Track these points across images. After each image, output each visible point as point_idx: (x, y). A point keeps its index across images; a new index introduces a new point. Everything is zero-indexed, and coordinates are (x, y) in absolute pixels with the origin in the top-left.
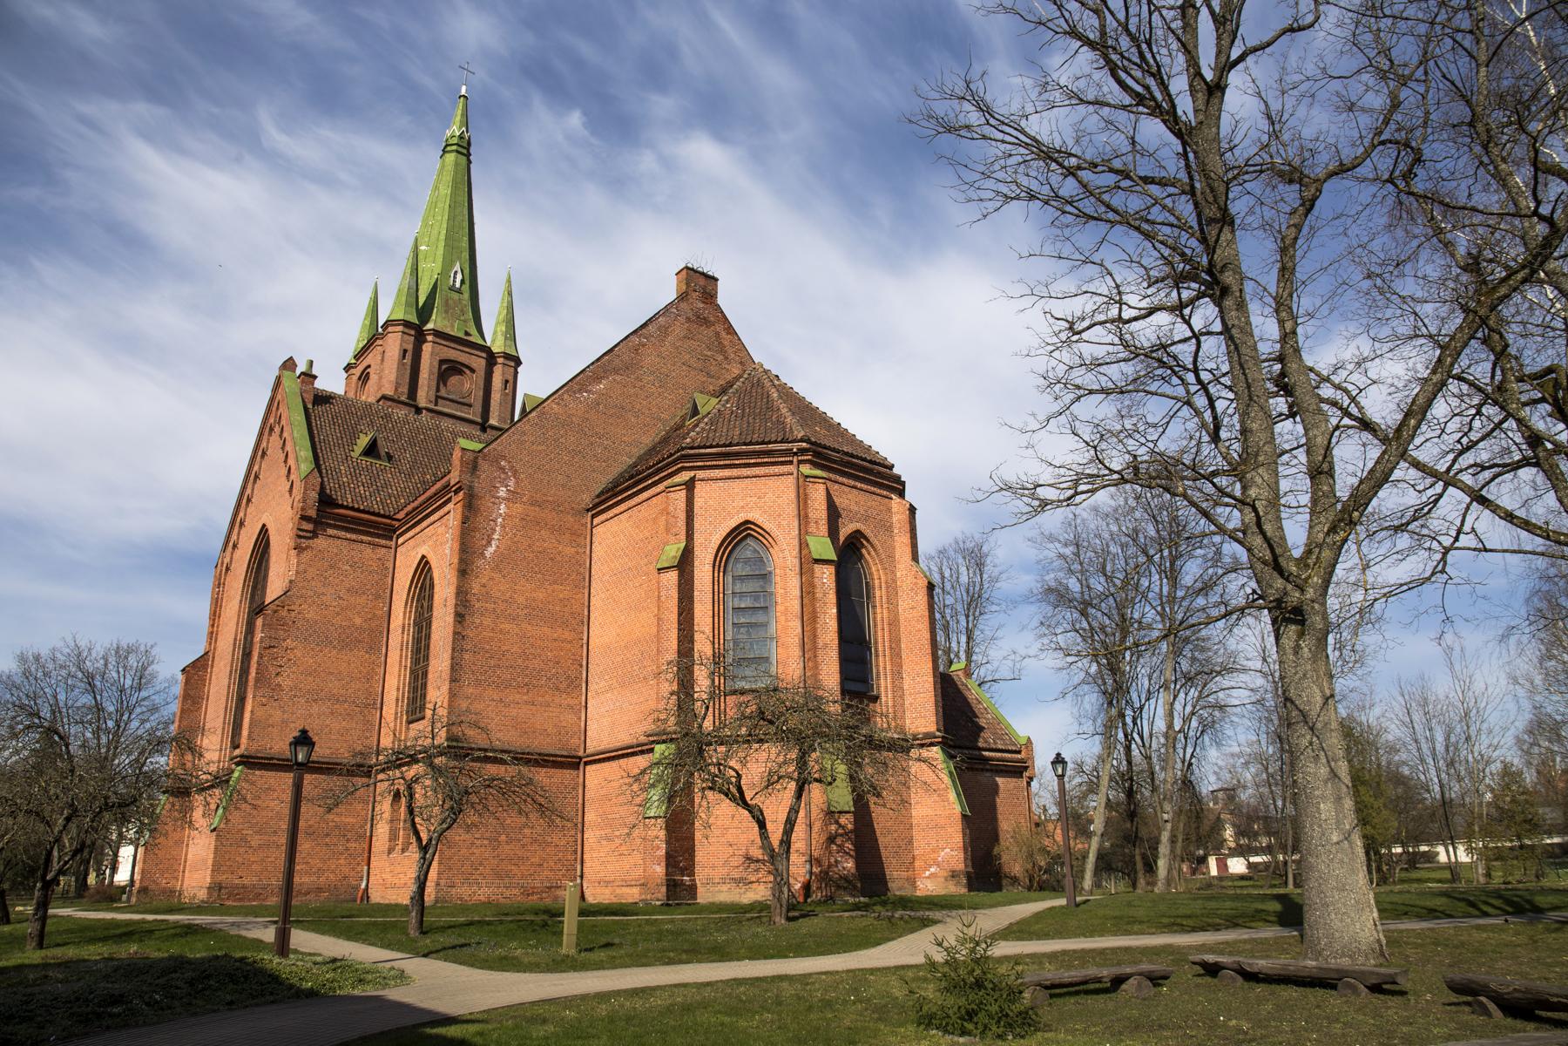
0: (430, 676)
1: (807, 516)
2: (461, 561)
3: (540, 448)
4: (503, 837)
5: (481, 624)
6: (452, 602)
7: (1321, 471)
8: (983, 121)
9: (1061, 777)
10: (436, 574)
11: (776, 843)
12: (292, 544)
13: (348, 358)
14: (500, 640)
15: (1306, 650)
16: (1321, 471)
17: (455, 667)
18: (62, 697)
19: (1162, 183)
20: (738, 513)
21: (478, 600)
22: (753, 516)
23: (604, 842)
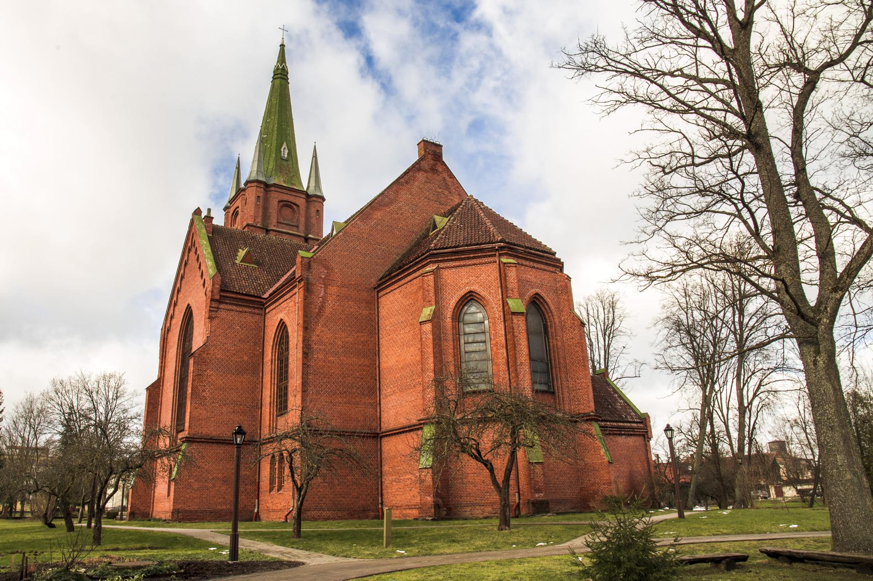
0: (289, 389)
1: (506, 287)
2: (304, 321)
3: (345, 253)
4: (336, 482)
5: (318, 358)
6: (301, 345)
7: (826, 254)
9: (670, 439)
10: (290, 330)
12: (207, 316)
14: (329, 367)
15: (821, 362)
16: (826, 254)
17: (305, 384)
18: (75, 404)
19: (715, 82)
20: (465, 286)
21: (315, 344)
22: (475, 288)
23: (394, 483)
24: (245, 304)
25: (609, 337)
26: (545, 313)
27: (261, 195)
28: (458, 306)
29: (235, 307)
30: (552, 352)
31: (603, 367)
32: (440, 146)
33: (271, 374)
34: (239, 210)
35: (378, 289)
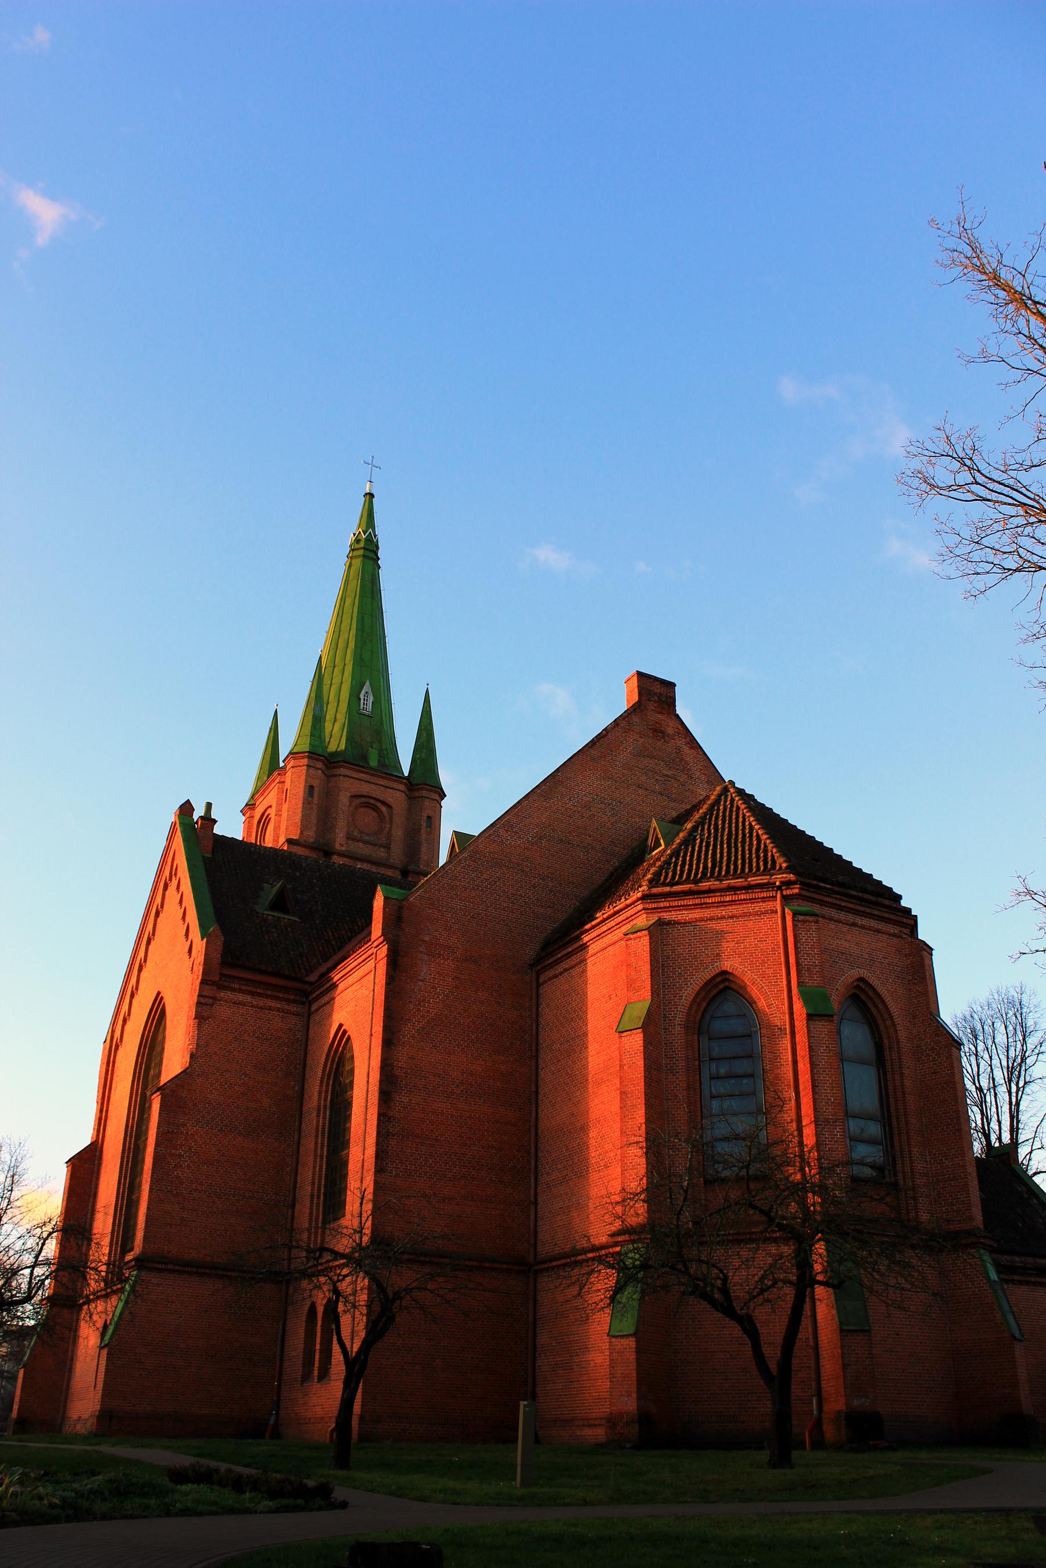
8: (970, 479)
11: (773, 1367)
13: (245, 798)
24: (269, 993)
25: (1017, 1084)
26: (879, 1021)
27: (316, 783)
28: (698, 1000)
29: (249, 998)
30: (892, 1100)
31: (1006, 1138)
32: (672, 686)
33: (317, 1136)
34: (272, 812)
35: (539, 967)
